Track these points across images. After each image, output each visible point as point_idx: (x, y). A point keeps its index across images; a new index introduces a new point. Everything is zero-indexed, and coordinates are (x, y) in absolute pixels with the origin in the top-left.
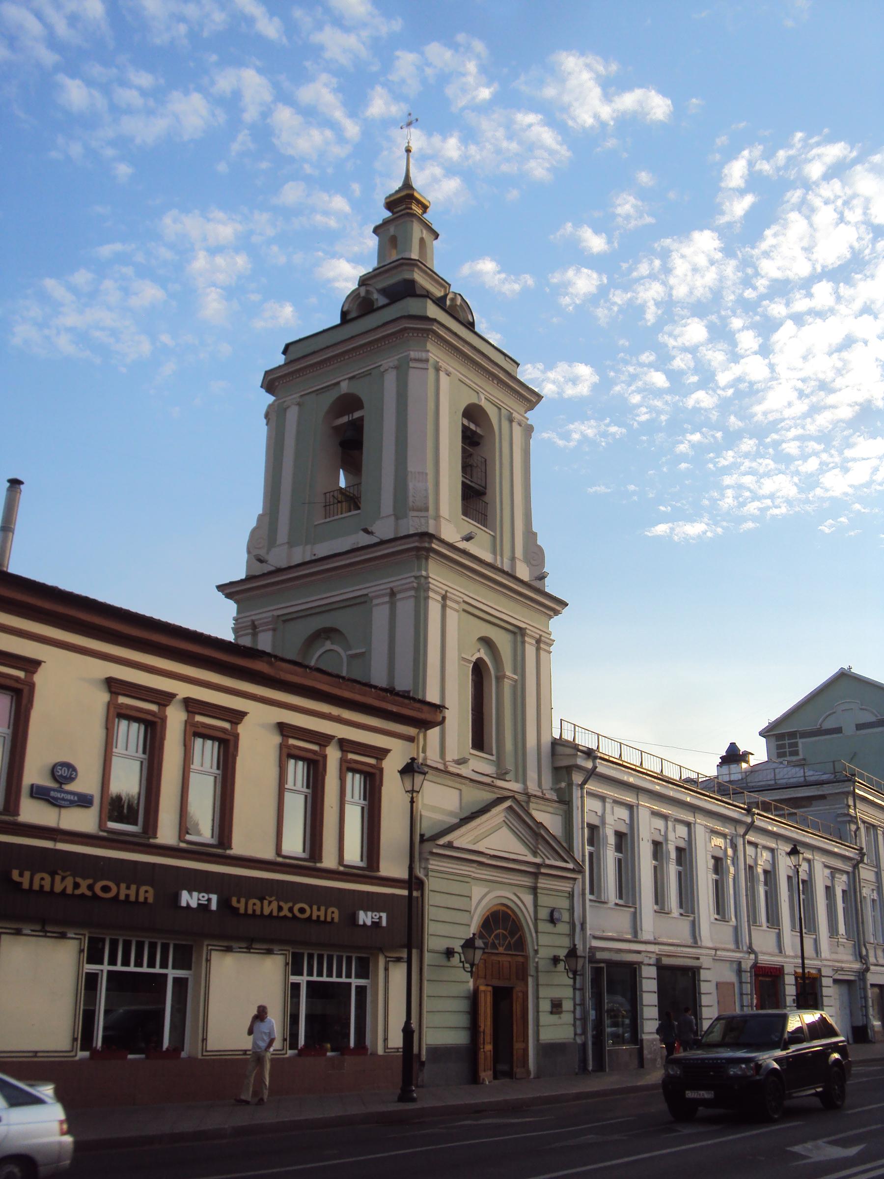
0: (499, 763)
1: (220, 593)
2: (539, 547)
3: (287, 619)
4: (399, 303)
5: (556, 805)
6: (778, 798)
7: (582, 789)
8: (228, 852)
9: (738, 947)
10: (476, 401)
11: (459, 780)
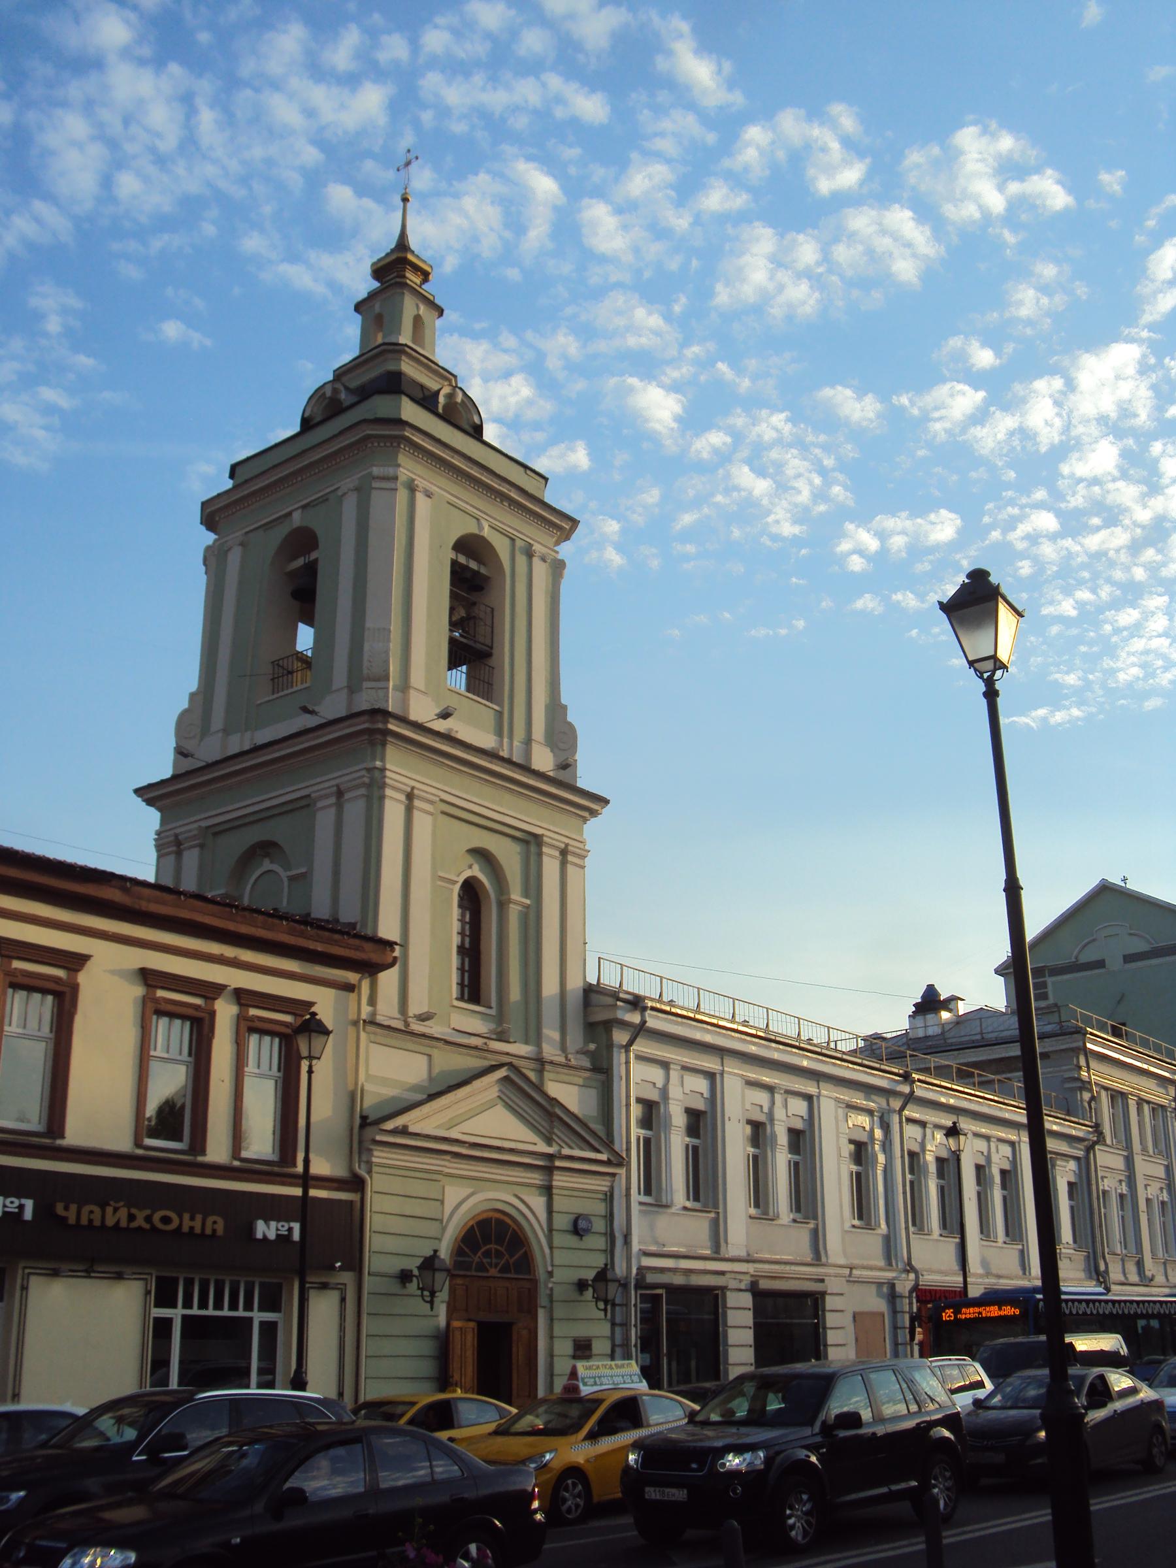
0: (500, 1018)
1: (140, 799)
2: (570, 724)
3: (217, 832)
4: (379, 402)
5: (587, 1074)
6: (965, 1061)
7: (627, 1051)
8: (59, 1142)
9: (890, 1264)
10: (476, 531)
11: (427, 1041)
